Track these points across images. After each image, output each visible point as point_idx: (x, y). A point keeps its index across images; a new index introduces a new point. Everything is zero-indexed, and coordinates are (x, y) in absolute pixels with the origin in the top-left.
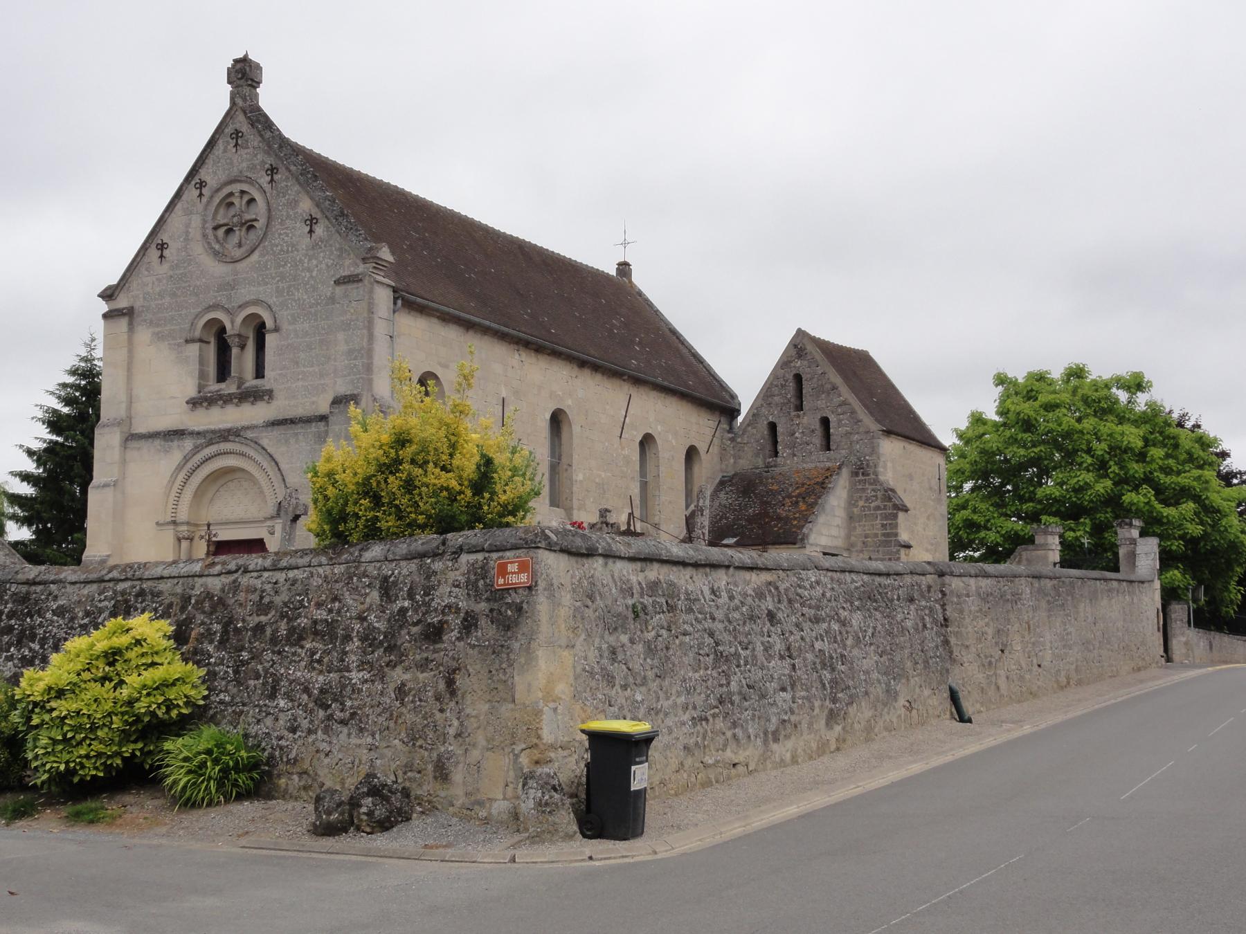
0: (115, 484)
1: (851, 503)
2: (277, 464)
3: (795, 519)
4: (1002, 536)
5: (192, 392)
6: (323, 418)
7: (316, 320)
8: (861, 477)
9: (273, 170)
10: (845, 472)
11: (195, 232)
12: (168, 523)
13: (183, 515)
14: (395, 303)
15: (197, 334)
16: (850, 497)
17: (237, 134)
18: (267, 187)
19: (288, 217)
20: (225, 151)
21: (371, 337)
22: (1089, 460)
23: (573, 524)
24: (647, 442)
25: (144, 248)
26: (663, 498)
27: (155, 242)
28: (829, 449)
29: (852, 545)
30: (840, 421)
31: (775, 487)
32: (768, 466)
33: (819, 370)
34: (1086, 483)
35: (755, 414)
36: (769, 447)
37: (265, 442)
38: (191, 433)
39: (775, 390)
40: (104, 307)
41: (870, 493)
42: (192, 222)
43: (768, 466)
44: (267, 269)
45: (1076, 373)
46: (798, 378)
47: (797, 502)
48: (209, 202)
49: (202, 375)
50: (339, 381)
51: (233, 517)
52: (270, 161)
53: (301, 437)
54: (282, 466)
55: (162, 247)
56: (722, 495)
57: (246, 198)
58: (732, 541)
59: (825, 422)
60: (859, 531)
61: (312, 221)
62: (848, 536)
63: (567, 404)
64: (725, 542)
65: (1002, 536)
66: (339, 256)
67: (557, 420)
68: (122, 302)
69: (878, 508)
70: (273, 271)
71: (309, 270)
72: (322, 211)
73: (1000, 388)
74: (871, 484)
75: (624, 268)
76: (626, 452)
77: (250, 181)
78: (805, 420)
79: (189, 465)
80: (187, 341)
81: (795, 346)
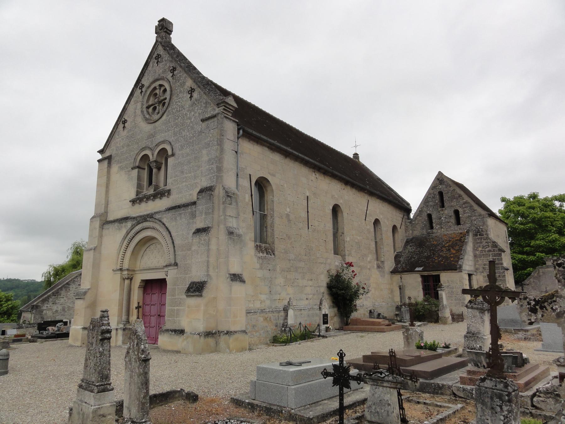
0: (95, 249)
1: (475, 249)
2: (170, 233)
3: (452, 257)
4: (517, 260)
5: (133, 196)
6: (194, 203)
7: (193, 146)
8: (479, 237)
9: (174, 69)
10: (471, 234)
11: (139, 112)
12: (118, 270)
13: (126, 266)
14: (238, 133)
15: (137, 164)
16: (474, 246)
17: (159, 56)
18: (171, 79)
19: (181, 92)
20: (153, 67)
21: (222, 151)
22: (555, 229)
23: (346, 264)
24: (377, 222)
25: (117, 124)
26: (385, 249)
27: (121, 120)
28: (460, 224)
29: (477, 269)
30: (464, 211)
31: (435, 243)
32: (429, 233)
33: (452, 189)
34: (556, 239)
35: (420, 211)
36: (428, 225)
37: (164, 220)
38: (131, 218)
39: (430, 200)
40: (100, 157)
41: (484, 243)
42: (137, 107)
43: (429, 233)
44: (170, 122)
45: (534, 196)
46: (441, 194)
47: (449, 250)
48: (144, 94)
49: (139, 186)
50: (203, 179)
51: (152, 266)
52: (173, 64)
53: (183, 216)
54: (173, 234)
55: (125, 122)
56: (409, 247)
57: (162, 89)
58: (421, 269)
59: (457, 213)
60: (480, 262)
61: (192, 91)
62: (475, 265)
63: (340, 202)
64: (417, 269)
65: (517, 260)
66: (206, 107)
67: (336, 210)
68: (107, 154)
69: (490, 251)
70: (172, 123)
71: (190, 118)
72: (197, 84)
73: (504, 203)
74: (484, 240)
75: (356, 155)
76: (368, 227)
77: (162, 79)
78: (446, 212)
79: (129, 236)
80: (132, 169)
81: (438, 179)
